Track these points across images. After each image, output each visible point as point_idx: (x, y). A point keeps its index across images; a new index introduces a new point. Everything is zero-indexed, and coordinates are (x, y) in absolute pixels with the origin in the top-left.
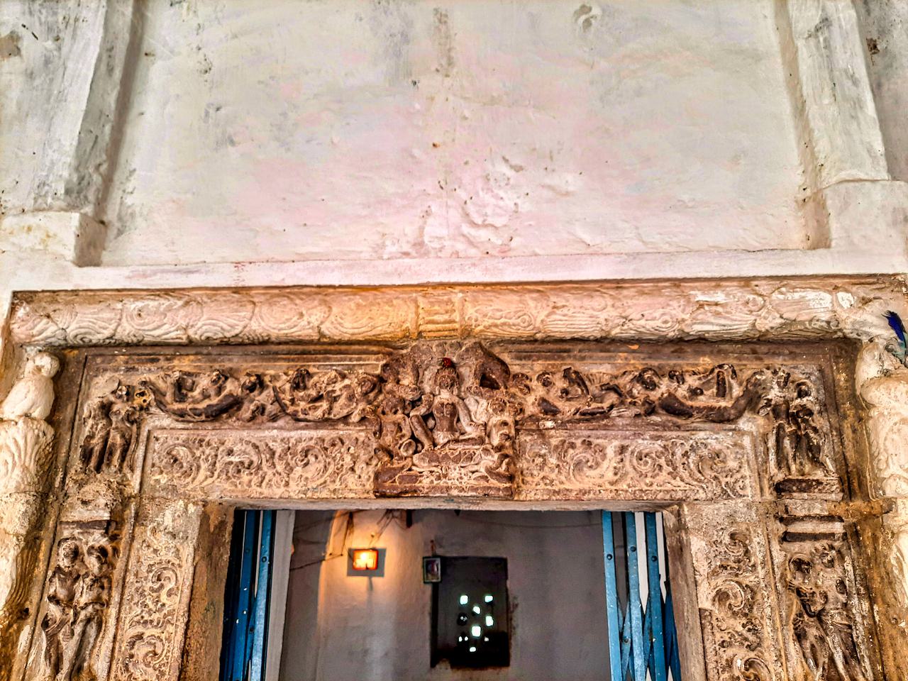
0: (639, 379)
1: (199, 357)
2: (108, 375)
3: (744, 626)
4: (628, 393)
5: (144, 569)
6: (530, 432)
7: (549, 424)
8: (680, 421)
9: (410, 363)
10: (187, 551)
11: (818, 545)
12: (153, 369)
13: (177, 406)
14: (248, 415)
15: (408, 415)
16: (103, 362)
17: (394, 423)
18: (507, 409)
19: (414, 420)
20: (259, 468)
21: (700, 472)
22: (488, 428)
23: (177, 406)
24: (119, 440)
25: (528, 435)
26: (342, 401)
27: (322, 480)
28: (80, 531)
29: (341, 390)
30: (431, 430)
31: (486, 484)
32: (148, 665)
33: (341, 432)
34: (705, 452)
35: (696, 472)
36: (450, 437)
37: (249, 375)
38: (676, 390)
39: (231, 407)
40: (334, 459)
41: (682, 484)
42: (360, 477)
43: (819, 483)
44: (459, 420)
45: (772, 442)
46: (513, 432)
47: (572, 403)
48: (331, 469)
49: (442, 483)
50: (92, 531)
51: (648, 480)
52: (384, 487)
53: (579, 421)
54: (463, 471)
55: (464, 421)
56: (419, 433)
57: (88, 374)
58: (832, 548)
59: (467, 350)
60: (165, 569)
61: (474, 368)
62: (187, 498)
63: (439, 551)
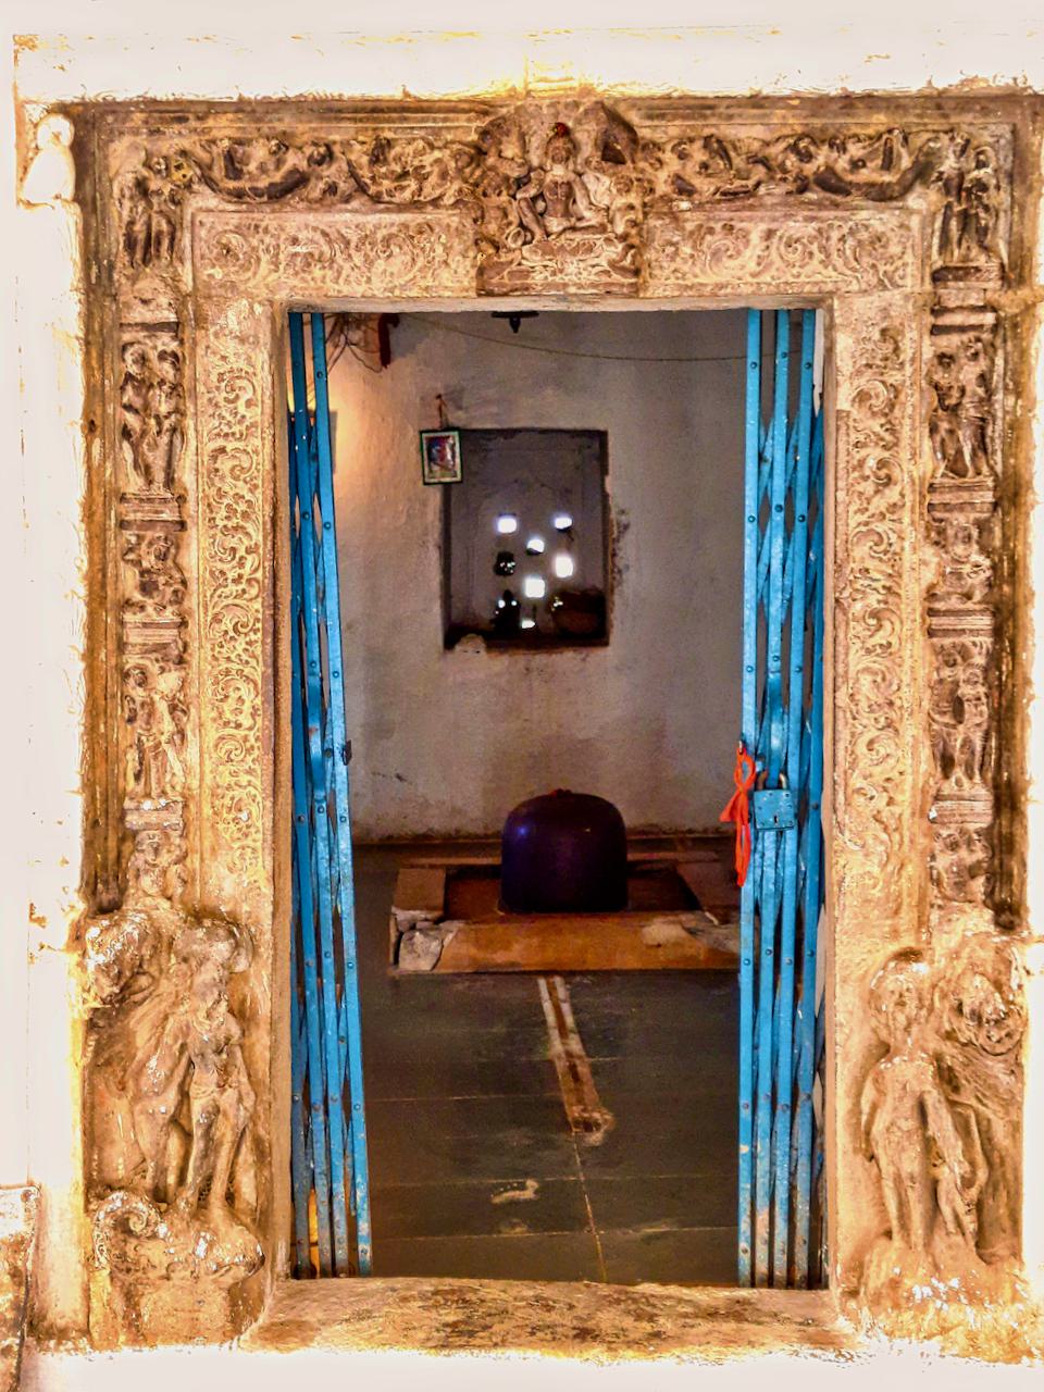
0: (794, 148)
1: (240, 116)
2: (127, 140)
3: (882, 426)
4: (779, 166)
5: (214, 378)
6: (660, 216)
7: (685, 205)
8: (839, 198)
9: (515, 130)
10: (262, 357)
11: (965, 337)
12: (183, 131)
13: (232, 184)
14: (316, 194)
15: (514, 197)
16: (116, 120)
17: (498, 208)
18: (634, 188)
19: (523, 204)
20: (332, 261)
21: (856, 260)
22: (611, 213)
23: (232, 184)
24: (165, 227)
25: (659, 218)
26: (433, 179)
27: (411, 276)
28: (145, 333)
29: (431, 165)
30: (542, 214)
31: (609, 280)
32: (237, 478)
33: (429, 217)
34: (864, 235)
35: (852, 259)
36: (566, 224)
37: (315, 144)
38: (836, 160)
39: (295, 183)
40: (423, 249)
41: (834, 274)
42: (456, 272)
43: (977, 269)
44: (574, 201)
45: (938, 224)
46: (641, 216)
47: (712, 180)
48: (421, 262)
49: (558, 279)
50: (159, 334)
51: (795, 271)
52: (491, 284)
53: (719, 201)
54: (582, 265)
55: (581, 206)
56: (529, 220)
57: (100, 138)
58: (978, 340)
59: (586, 112)
60: (237, 377)
61: (593, 135)
62: (250, 296)
63: (457, 417)
